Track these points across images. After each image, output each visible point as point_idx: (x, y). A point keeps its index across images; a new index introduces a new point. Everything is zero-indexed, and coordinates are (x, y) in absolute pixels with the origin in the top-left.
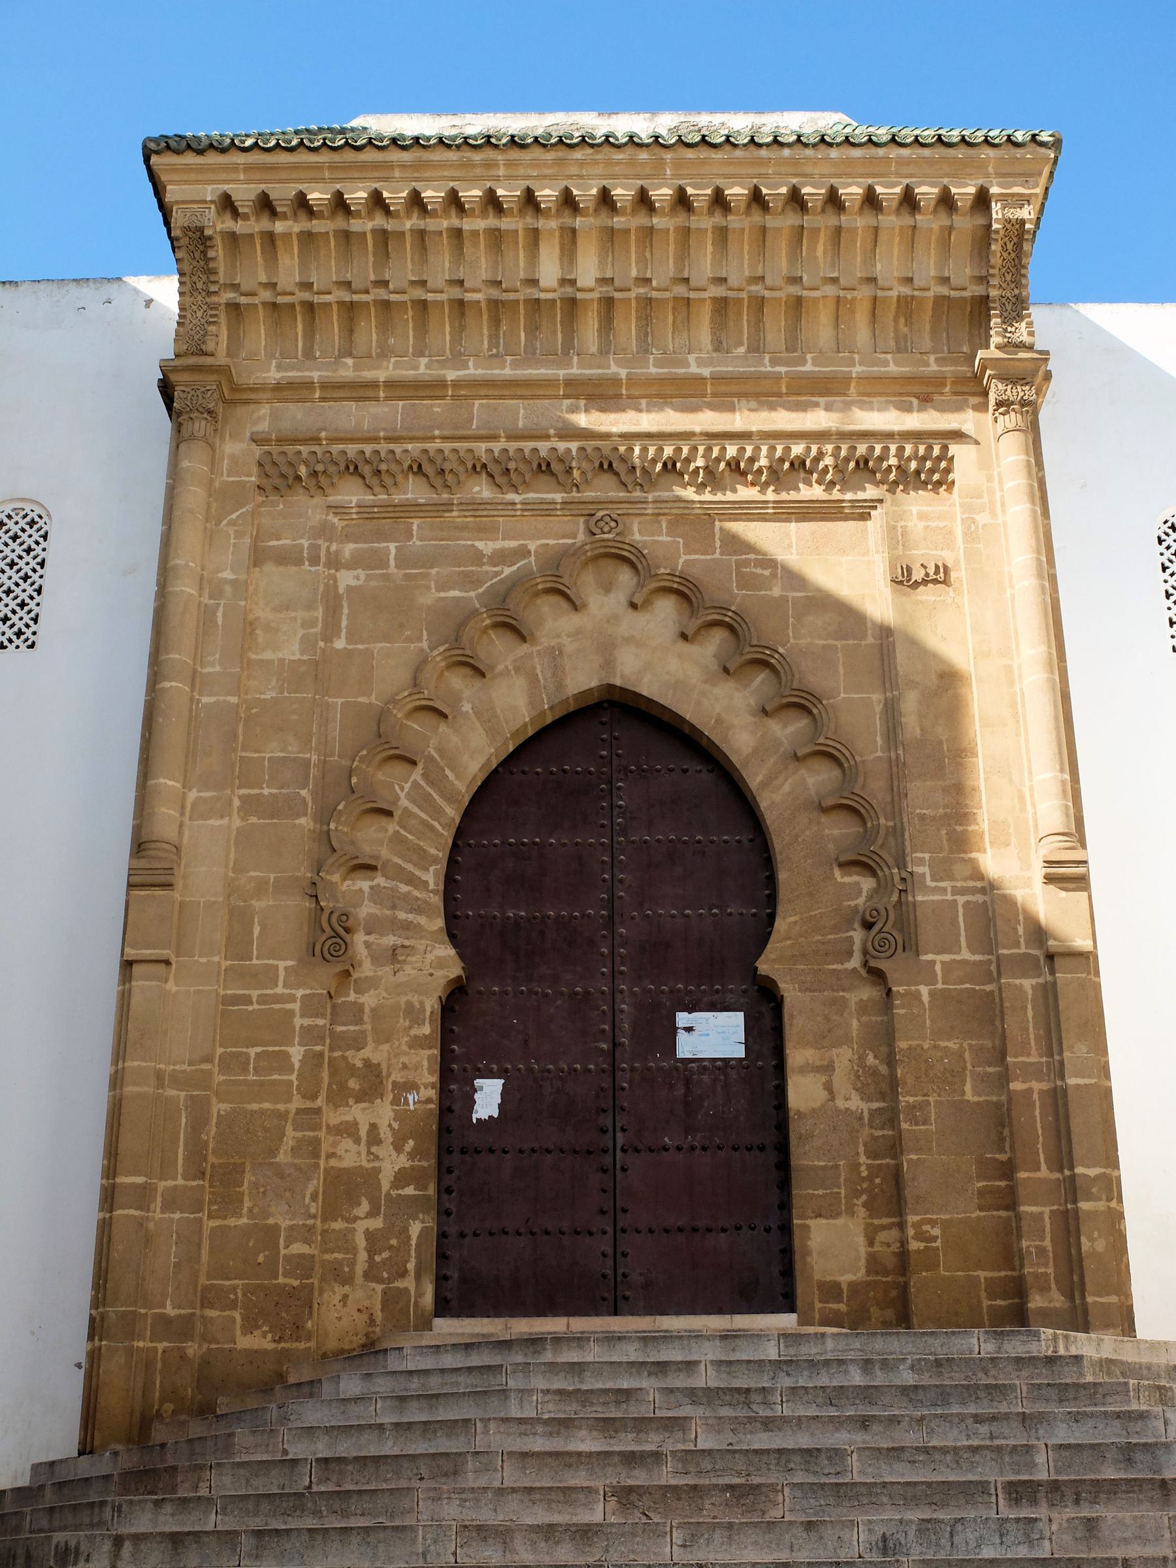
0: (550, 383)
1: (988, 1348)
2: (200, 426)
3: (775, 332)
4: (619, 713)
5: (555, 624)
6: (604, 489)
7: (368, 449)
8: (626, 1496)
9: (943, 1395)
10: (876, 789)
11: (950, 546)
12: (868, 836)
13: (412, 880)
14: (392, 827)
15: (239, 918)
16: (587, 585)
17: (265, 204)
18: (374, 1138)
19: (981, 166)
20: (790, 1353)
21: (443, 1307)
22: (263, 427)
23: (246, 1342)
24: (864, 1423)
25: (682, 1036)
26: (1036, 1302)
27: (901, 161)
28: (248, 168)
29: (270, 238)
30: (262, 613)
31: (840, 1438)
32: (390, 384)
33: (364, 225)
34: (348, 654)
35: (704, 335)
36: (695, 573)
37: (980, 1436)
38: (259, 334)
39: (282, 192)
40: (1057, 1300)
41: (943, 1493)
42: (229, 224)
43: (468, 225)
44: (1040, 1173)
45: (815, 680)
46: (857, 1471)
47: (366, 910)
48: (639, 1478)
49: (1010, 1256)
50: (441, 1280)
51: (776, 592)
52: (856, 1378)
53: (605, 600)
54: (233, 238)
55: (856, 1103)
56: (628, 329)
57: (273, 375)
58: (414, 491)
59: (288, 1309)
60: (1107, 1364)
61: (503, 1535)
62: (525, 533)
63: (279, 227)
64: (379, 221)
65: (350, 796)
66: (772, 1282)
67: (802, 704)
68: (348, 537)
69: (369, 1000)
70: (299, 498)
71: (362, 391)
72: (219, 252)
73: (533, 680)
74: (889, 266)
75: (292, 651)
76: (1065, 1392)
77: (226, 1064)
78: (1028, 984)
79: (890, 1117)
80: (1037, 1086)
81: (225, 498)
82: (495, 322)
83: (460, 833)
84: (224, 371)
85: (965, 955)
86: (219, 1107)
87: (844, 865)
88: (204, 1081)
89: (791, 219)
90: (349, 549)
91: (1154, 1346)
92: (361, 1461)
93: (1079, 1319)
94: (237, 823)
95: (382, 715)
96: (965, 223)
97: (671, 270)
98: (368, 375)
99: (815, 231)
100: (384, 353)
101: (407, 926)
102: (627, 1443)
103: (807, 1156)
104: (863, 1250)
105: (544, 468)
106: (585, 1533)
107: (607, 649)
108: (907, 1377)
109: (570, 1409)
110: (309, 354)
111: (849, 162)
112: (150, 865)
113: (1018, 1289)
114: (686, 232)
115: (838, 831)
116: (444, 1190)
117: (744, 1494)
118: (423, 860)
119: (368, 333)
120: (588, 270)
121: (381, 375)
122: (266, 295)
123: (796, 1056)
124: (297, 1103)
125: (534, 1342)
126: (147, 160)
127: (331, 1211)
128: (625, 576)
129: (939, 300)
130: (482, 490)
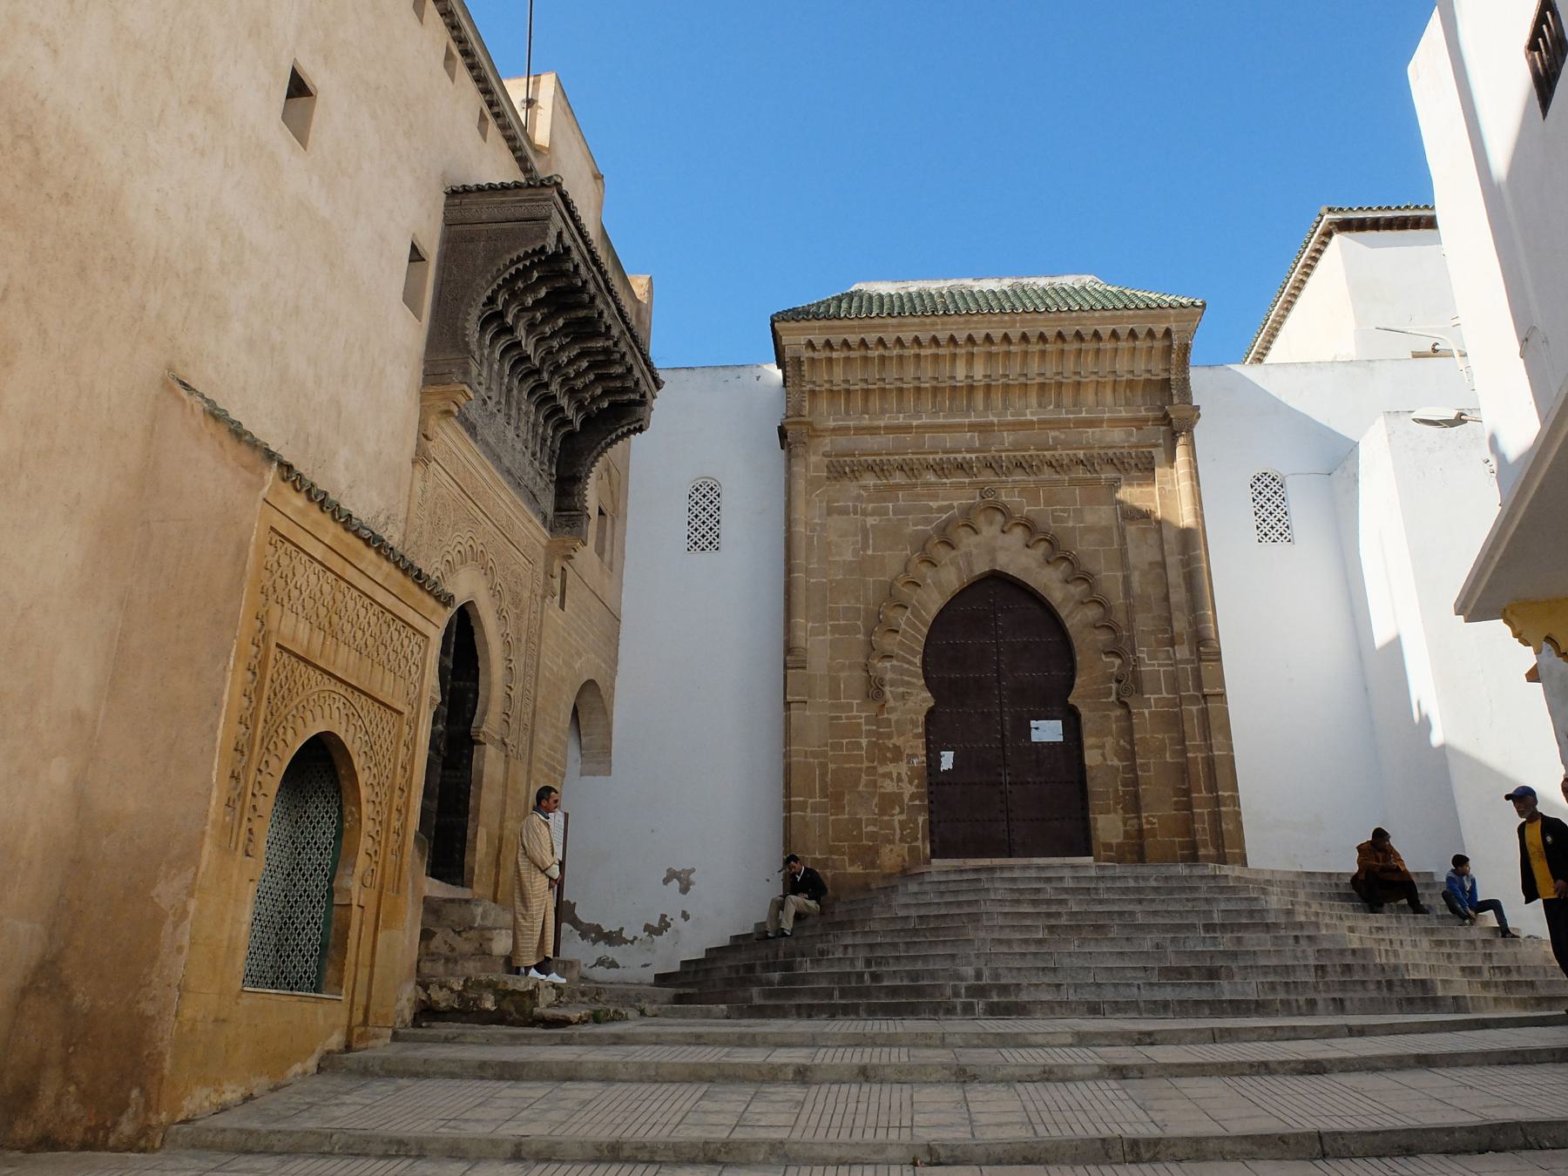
0: (961, 426)
1: (1186, 872)
2: (800, 450)
3: (1067, 398)
4: (998, 583)
5: (967, 541)
6: (987, 476)
7: (877, 459)
8: (1051, 929)
9: (1171, 891)
10: (1120, 617)
11: (1153, 500)
12: (1117, 639)
13: (910, 663)
14: (899, 637)
15: (834, 682)
16: (981, 522)
17: (828, 344)
18: (900, 779)
19: (1167, 318)
20: (1100, 873)
21: (934, 854)
22: (828, 448)
23: (851, 870)
24: (1140, 901)
25: (1033, 732)
26: (1202, 852)
27: (1129, 317)
28: (820, 328)
29: (830, 360)
30: (834, 538)
31: (1130, 908)
32: (886, 427)
33: (875, 353)
34: (873, 557)
35: (1034, 401)
36: (1032, 516)
37: (1189, 906)
38: (823, 404)
39: (836, 339)
40: (1212, 851)
41: (1179, 927)
42: (810, 354)
43: (923, 352)
44: (1203, 794)
45: (1088, 565)
46: (1140, 919)
47: (889, 676)
48: (1053, 922)
49: (1190, 832)
50: (932, 842)
51: (1071, 524)
52: (1132, 884)
53: (990, 530)
54: (812, 360)
55: (1116, 762)
56: (997, 399)
57: (832, 424)
58: (899, 478)
59: (868, 855)
60: (1238, 878)
61: (1009, 942)
62: (953, 496)
63: (835, 355)
64: (881, 351)
65: (879, 623)
66: (1083, 845)
67: (1085, 578)
68: (870, 501)
69: (893, 717)
70: (846, 482)
71: (873, 430)
72: (805, 368)
73: (959, 569)
74: (1122, 365)
75: (849, 556)
76: (1222, 890)
77: (834, 747)
78: (1194, 708)
79: (1133, 769)
80: (1200, 755)
81: (813, 483)
82: (935, 396)
83: (928, 638)
84: (810, 424)
85: (1165, 695)
86: (831, 766)
87: (1107, 653)
88: (824, 754)
89: (1076, 345)
90: (871, 506)
91: (1258, 871)
92: (937, 917)
93: (1222, 859)
94: (829, 637)
95: (891, 586)
96: (1159, 344)
97: (1018, 370)
98: (876, 423)
99: (1087, 351)
100: (883, 411)
101: (909, 684)
102: (1043, 909)
103: (1095, 786)
104: (1122, 829)
105: (960, 467)
106: (1040, 942)
107: (992, 551)
108: (1154, 884)
109: (1016, 896)
110: (847, 412)
111: (1104, 318)
112: (792, 657)
113: (1193, 846)
114: (1026, 353)
115: (1103, 637)
116: (931, 802)
117: (1097, 928)
118: (913, 652)
119: (875, 402)
120: (979, 371)
121: (882, 423)
122: (827, 386)
123: (1088, 741)
124: (866, 764)
125: (991, 869)
126: (772, 326)
127: (883, 811)
128: (999, 518)
129: (1148, 381)
130: (931, 477)
